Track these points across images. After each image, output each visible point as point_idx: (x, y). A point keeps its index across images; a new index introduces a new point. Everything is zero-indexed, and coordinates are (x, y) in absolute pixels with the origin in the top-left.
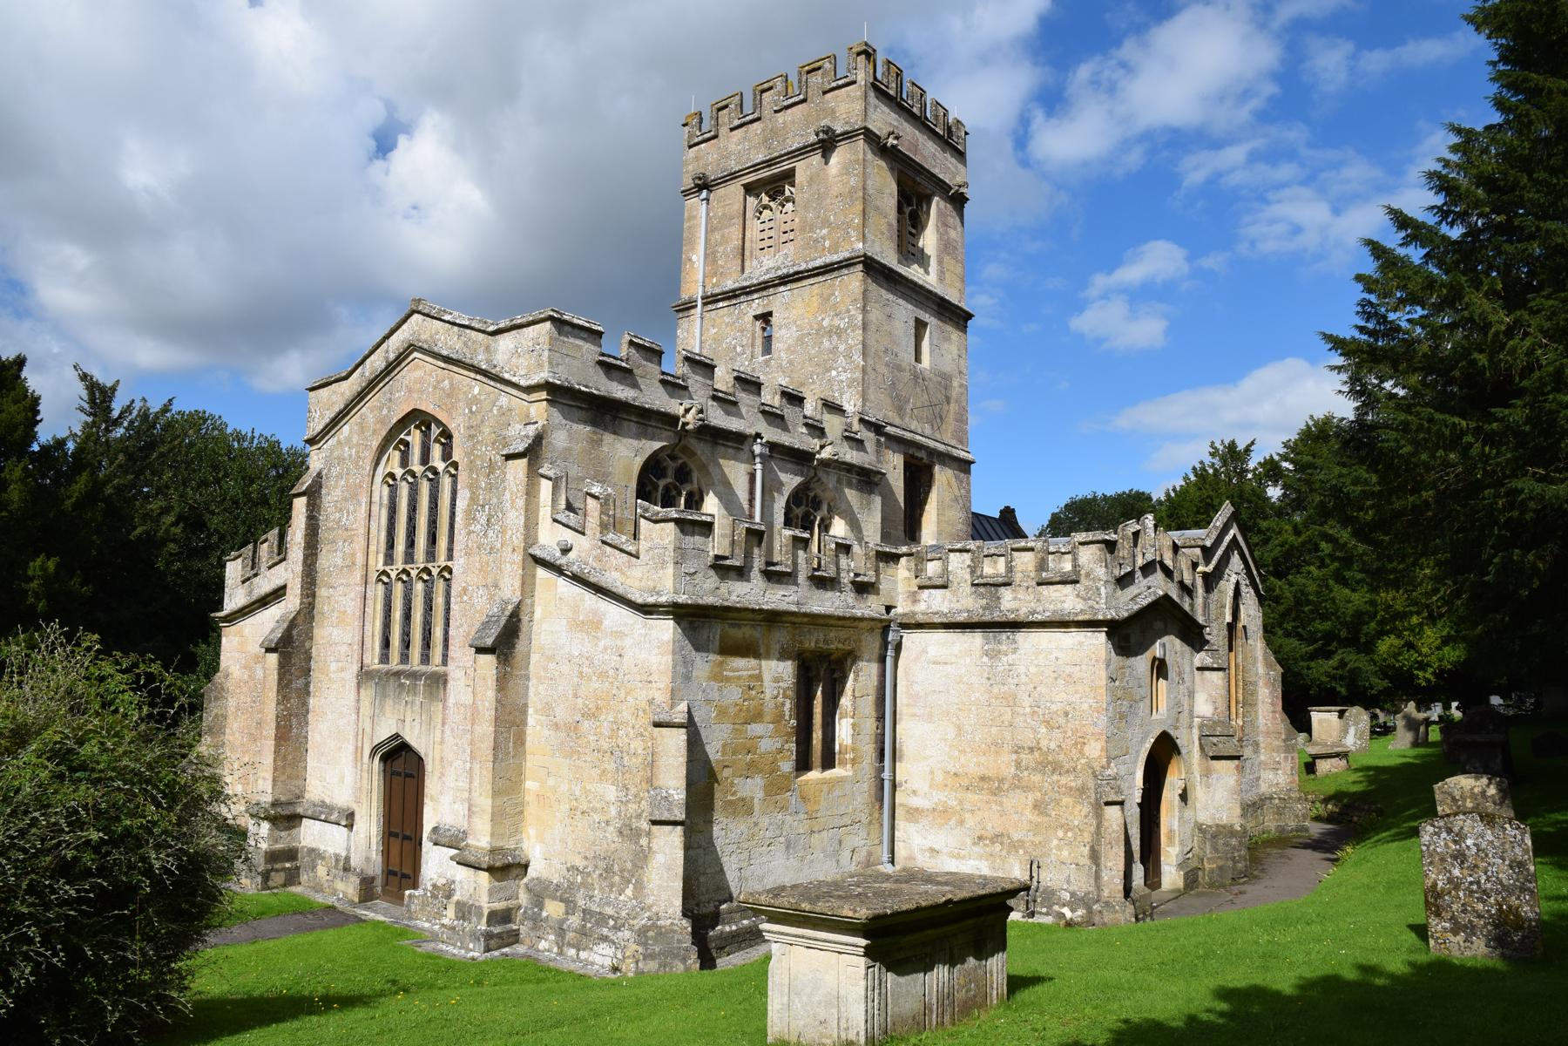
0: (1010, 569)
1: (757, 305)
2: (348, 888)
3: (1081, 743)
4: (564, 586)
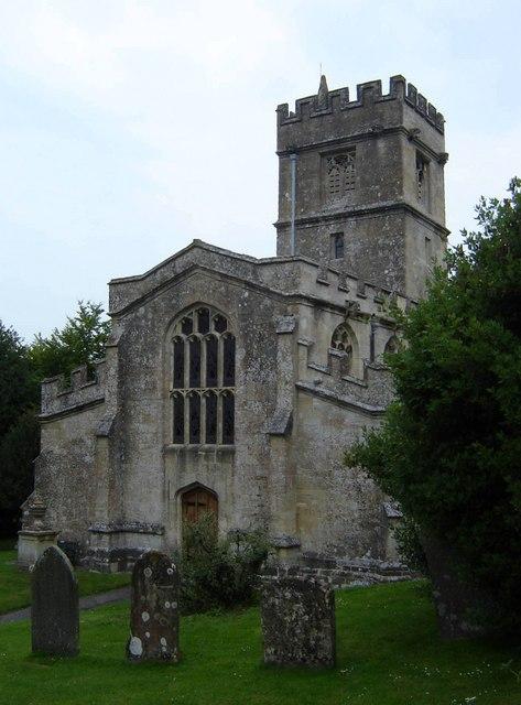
4: (316, 402)
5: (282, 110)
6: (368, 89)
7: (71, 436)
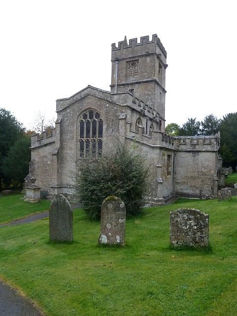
4: (132, 143)
5: (113, 45)
6: (145, 39)
7: (42, 155)
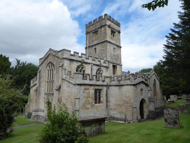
0: (121, 78)
1: (94, 47)
2: (43, 120)
3: (131, 100)
4: (66, 82)
